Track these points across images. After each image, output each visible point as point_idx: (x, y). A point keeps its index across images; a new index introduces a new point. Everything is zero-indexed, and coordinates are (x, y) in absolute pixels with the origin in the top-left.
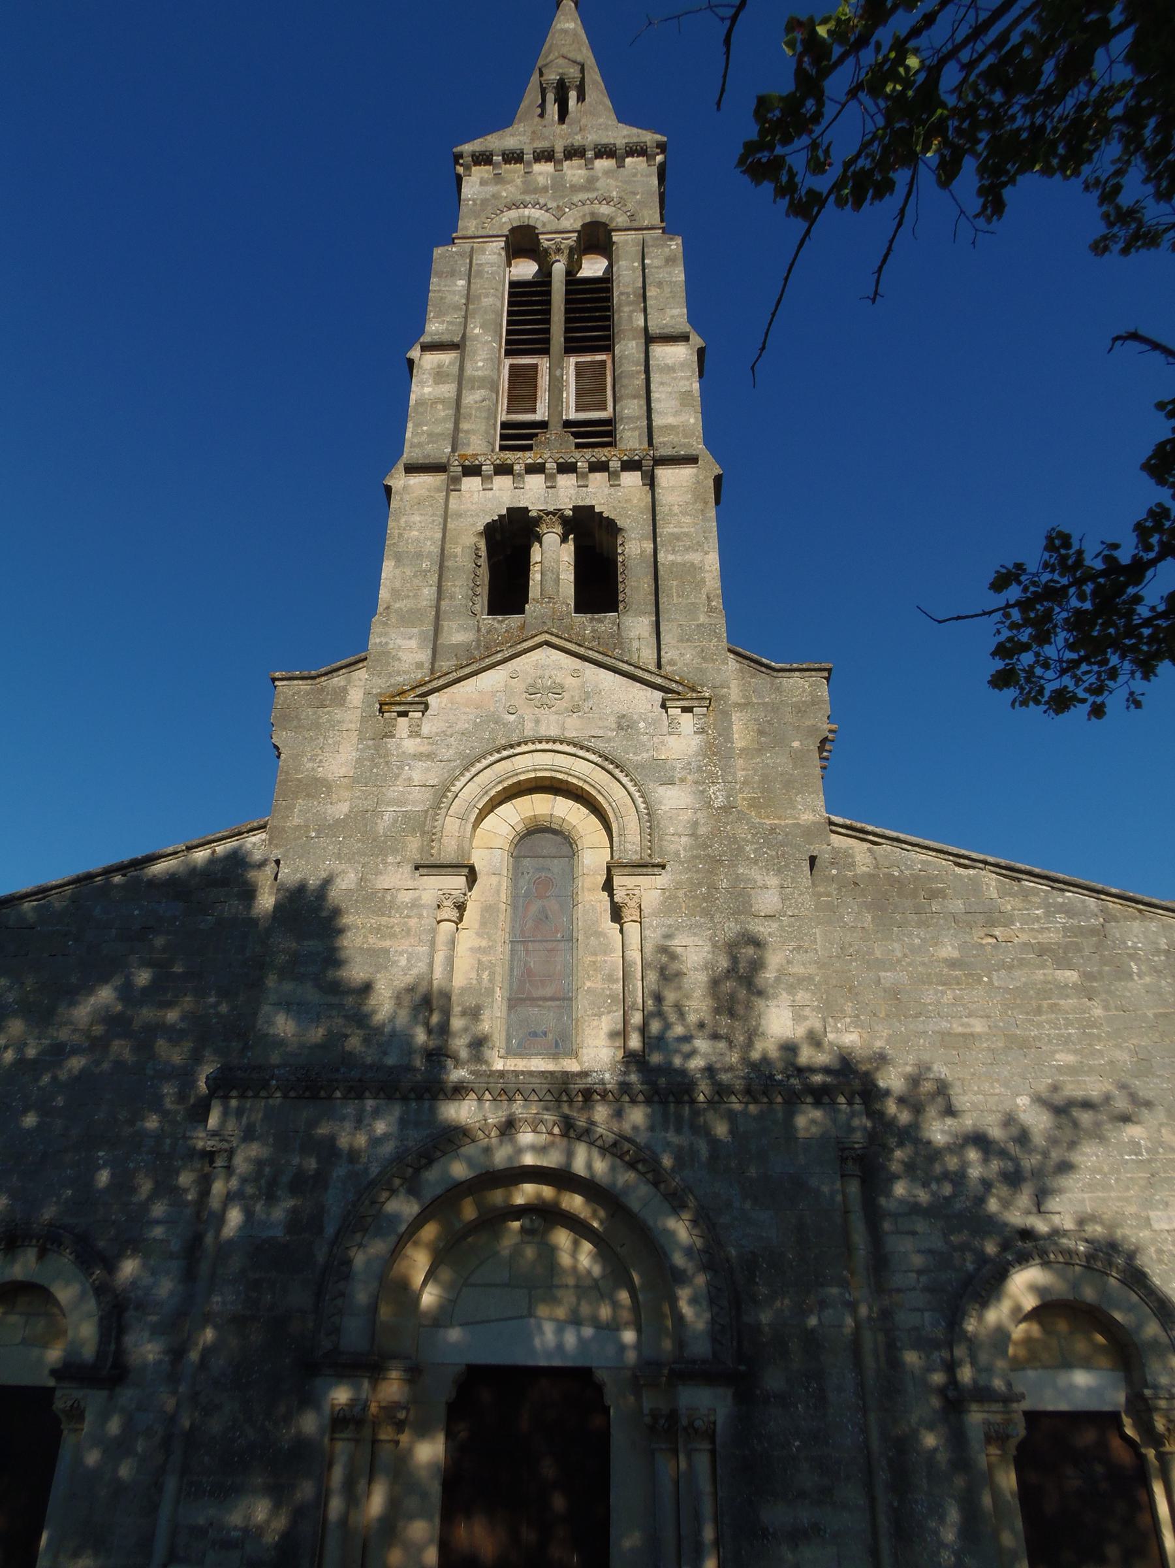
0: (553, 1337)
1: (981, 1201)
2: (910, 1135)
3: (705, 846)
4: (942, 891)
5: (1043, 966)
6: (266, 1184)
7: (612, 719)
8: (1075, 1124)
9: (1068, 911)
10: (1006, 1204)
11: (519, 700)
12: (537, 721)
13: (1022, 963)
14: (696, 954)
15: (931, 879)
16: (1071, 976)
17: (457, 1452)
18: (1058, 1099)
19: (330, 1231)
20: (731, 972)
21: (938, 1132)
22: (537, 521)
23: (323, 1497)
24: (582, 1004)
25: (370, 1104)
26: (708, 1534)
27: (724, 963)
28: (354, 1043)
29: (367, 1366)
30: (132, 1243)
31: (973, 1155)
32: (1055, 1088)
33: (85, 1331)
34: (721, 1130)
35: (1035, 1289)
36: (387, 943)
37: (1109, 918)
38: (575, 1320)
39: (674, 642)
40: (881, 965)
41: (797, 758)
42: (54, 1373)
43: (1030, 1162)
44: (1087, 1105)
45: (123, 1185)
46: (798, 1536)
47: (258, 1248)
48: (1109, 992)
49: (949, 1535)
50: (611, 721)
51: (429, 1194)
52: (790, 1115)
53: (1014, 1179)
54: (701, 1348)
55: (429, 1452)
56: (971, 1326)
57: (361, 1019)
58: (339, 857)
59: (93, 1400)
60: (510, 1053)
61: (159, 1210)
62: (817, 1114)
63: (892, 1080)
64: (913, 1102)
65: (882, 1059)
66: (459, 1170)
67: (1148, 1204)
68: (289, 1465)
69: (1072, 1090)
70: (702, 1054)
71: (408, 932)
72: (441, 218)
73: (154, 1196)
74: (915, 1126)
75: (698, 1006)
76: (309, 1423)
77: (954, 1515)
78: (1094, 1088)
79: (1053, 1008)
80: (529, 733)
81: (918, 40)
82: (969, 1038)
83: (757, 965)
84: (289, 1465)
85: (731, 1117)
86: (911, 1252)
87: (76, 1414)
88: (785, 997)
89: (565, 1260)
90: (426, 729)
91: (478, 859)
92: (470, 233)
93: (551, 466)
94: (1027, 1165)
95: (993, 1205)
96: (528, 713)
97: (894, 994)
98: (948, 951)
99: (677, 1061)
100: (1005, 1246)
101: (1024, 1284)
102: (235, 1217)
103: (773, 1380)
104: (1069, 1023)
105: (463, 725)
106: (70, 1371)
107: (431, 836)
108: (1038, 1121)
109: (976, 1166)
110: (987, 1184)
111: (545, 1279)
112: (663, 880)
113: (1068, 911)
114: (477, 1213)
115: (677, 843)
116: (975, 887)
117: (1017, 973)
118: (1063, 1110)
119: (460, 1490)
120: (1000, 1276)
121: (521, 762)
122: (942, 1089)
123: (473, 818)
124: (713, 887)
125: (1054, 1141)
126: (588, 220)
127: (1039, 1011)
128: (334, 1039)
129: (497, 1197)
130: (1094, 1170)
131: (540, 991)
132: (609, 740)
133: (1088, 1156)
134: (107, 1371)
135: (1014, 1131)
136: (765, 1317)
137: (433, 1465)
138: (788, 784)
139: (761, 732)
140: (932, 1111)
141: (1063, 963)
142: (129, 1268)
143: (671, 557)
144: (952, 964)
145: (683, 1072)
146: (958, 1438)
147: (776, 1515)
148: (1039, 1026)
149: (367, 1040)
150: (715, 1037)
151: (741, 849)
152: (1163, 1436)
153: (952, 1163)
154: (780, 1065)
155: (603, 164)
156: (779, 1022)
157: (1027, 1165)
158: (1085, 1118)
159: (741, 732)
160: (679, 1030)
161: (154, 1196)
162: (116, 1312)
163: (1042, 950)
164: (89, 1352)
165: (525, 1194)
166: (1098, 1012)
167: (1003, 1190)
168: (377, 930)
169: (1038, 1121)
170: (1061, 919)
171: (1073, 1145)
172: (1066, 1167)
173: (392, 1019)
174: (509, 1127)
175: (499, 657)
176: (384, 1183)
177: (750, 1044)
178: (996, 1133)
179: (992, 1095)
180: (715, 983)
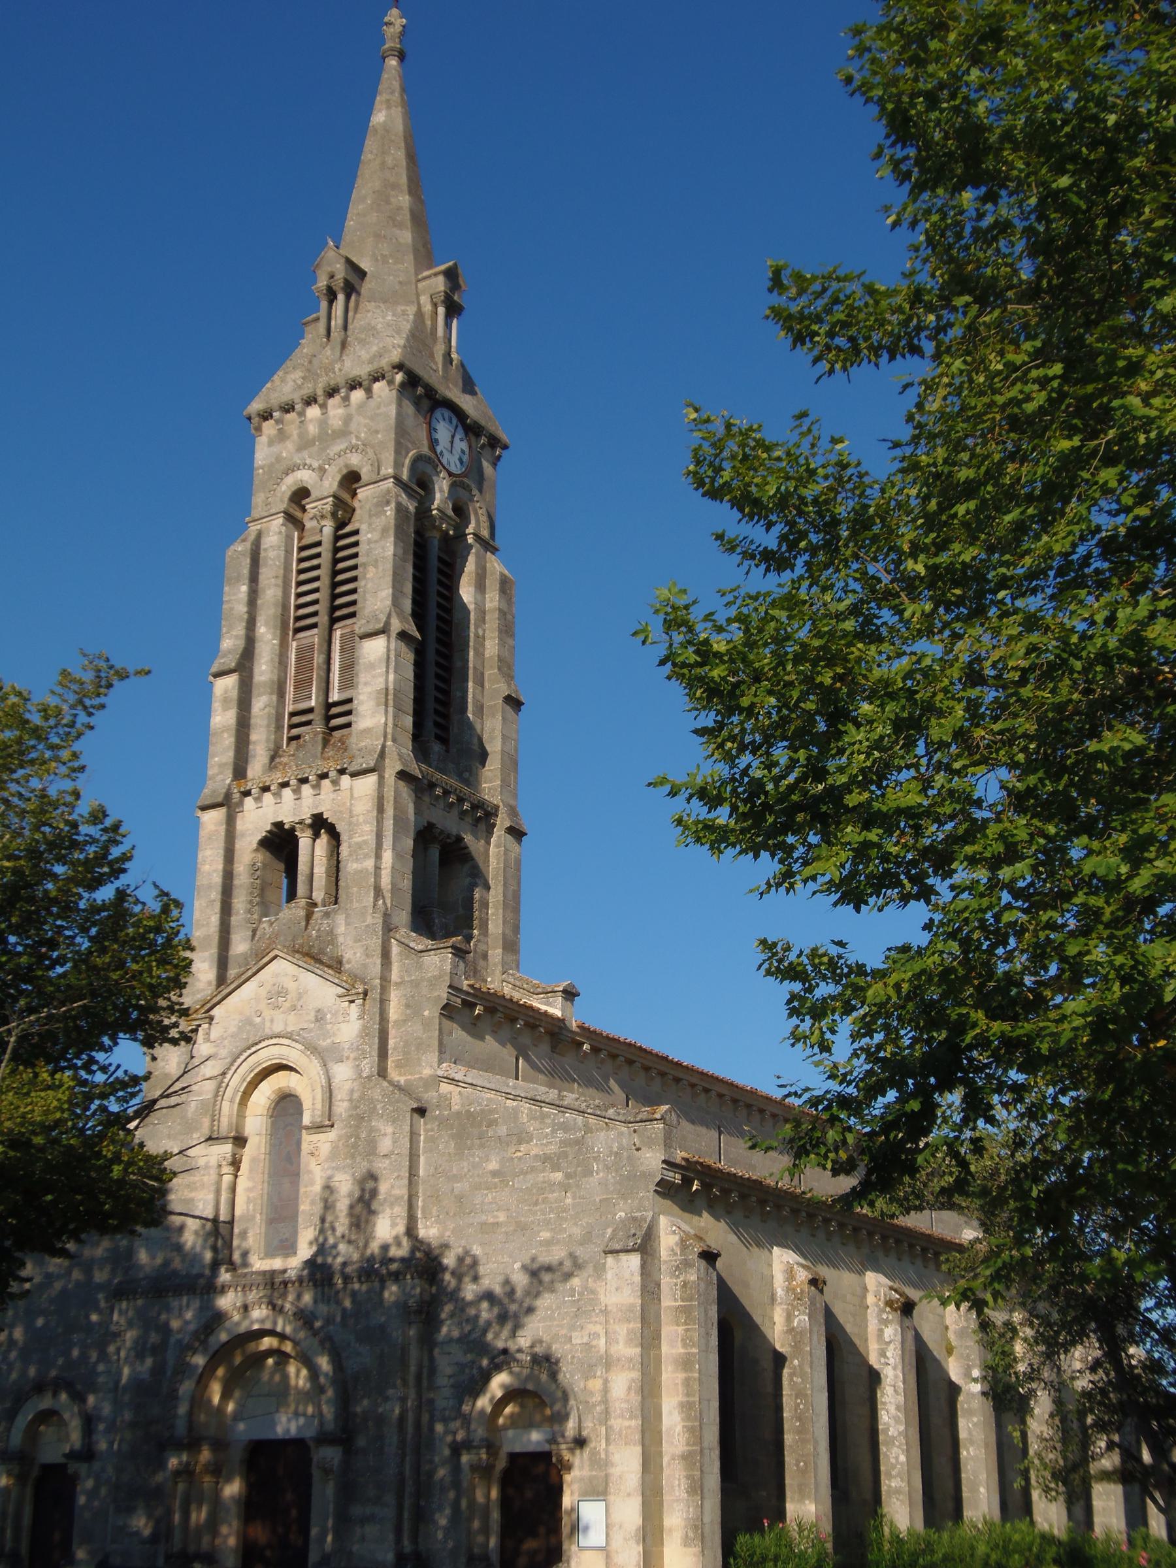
0: (286, 1425)
1: (485, 1332)
2: (454, 1295)
3: (356, 1107)
4: (496, 1120)
5: (543, 1171)
6: (140, 1351)
7: (313, 1014)
8: (541, 1282)
9: (565, 1127)
10: (497, 1335)
11: (263, 1006)
12: (272, 1021)
13: (533, 1169)
14: (345, 1185)
15: (492, 1111)
16: (558, 1176)
17: (252, 1488)
18: (535, 1266)
19: (169, 1373)
20: (361, 1199)
21: (469, 1291)
22: (293, 829)
23: (169, 1512)
24: (301, 1226)
25: (185, 1299)
26: (330, 1523)
27: (357, 1194)
28: (177, 1264)
29: (192, 1444)
30: (92, 1387)
31: (485, 1305)
32: (533, 1260)
33: (75, 1437)
34: (347, 1303)
35: (503, 1386)
36: (193, 1195)
37: (588, 1129)
38: (296, 1414)
39: (350, 943)
41: (426, 1024)
42: (65, 1455)
43: (513, 1307)
44: (549, 1269)
45: (84, 1356)
46: (365, 1520)
47: (137, 1384)
48: (578, 1186)
49: (443, 1522)
50: (312, 1017)
51: (211, 1351)
52: (383, 1288)
53: (503, 1318)
54: (330, 1426)
55: (232, 1489)
56: (466, 1408)
57: (179, 1248)
58: (169, 1137)
59: (83, 1468)
60: (269, 1254)
61: (101, 1368)
62: (394, 1288)
63: (449, 1260)
64: (458, 1275)
65: (446, 1246)
66: (224, 1337)
67: (573, 1328)
68: (155, 1497)
69: (545, 1259)
70: (345, 1252)
71: (203, 1186)
72: (240, 476)
73: (98, 1361)
74: (458, 1289)
75: (342, 1225)
76: (159, 1477)
77: (448, 1511)
78: (556, 1254)
79: (545, 1200)
80: (268, 1032)
82: (497, 1224)
83: (374, 1193)
84: (155, 1497)
85: (354, 1294)
86: (445, 1367)
88: (388, 1210)
89: (293, 1382)
90: (213, 1036)
92: (257, 516)
93: (293, 782)
94: (510, 1309)
95: (490, 1336)
96: (267, 1014)
97: (460, 1199)
98: (493, 1165)
99: (330, 1260)
100: (492, 1360)
101: (499, 1382)
102: (126, 1371)
103: (361, 1442)
104: (551, 1211)
105: (233, 1029)
106: (73, 1455)
107: (215, 1118)
108: (521, 1280)
109: (486, 1312)
110: (489, 1324)
111: (282, 1392)
112: (332, 1135)
113: (565, 1127)
114: (241, 1357)
116: (516, 1111)
117: (529, 1177)
118: (534, 1273)
119: (250, 1507)
120: (486, 1378)
121: (263, 1054)
122: (475, 1263)
123: (238, 1099)
124: (358, 1137)
125: (527, 1293)
126: (345, 471)
127: (536, 1204)
128: (166, 1263)
129: (252, 1347)
130: (547, 1309)
131: (281, 1214)
132: (311, 1031)
133: (545, 1302)
134: (87, 1454)
135: (508, 1289)
136: (359, 1409)
137: (232, 1498)
138: (419, 1047)
139: (408, 1006)
140: (467, 1279)
141: (556, 1168)
142: (91, 1400)
143: (355, 866)
144: (495, 1174)
145: (330, 1266)
146: (456, 1469)
147: (357, 1510)
148: (535, 1213)
149: (183, 1261)
150: (350, 1242)
151: (375, 1108)
153: (472, 1312)
154: (378, 1259)
155: (358, 395)
156: (386, 1228)
157: (510, 1309)
158: (546, 1277)
160: (331, 1241)
161: (98, 1361)
162: (89, 1422)
163: (545, 1159)
164: (78, 1445)
165: (267, 1343)
166: (569, 1201)
167: (496, 1327)
168: (188, 1186)
169: (521, 1280)
170: (560, 1134)
171: (537, 1295)
172: (530, 1310)
173: (193, 1248)
174: (246, 1308)
175: (250, 973)
176: (187, 1348)
177: (366, 1245)
178: (498, 1290)
179: (501, 1268)
180: (351, 1207)
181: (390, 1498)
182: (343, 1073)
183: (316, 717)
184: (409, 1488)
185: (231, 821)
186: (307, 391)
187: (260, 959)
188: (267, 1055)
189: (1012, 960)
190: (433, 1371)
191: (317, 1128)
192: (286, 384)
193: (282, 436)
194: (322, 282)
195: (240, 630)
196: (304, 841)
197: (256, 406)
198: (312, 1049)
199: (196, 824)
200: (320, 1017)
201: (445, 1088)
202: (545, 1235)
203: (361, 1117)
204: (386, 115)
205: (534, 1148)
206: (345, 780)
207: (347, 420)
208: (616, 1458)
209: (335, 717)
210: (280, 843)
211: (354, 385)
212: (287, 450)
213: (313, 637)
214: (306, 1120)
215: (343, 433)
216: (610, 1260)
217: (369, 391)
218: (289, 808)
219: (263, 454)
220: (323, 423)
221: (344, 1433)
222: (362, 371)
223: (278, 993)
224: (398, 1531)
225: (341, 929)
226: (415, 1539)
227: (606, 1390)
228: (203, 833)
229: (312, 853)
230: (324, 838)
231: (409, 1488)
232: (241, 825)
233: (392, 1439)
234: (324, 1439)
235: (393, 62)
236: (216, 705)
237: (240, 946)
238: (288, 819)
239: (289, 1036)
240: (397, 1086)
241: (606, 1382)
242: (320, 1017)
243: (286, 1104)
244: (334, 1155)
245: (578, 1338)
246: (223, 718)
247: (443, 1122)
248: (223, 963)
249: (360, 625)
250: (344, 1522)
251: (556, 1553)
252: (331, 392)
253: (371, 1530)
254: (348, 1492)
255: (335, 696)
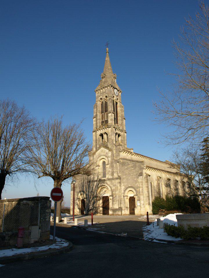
9: (133, 163)
16: (133, 168)
40: (122, 169)
46: (115, 204)
72: (95, 98)
81: (58, 238)
87: (3, 216)
91: (100, 165)
98: (126, 168)
103: (114, 196)
113: (133, 163)
115: (110, 162)
116: (128, 162)
141: (133, 168)
144: (126, 168)
147: (114, 203)
152: (103, 199)
155: (106, 88)
159: (114, 152)
181: (118, 202)
182: (110, 159)
183: (104, 122)
184: (119, 201)
185: (96, 133)
186: (101, 88)
187: (100, 148)
188: (102, 157)
189: (192, 169)
190: (121, 189)
191: (107, 165)
192: (99, 87)
193: (98, 93)
194: (102, 77)
195: (95, 113)
196: (104, 135)
197: (96, 90)
198: (106, 156)
199: (93, 134)
200: (107, 153)
201: (120, 160)
202: (132, 175)
203: (112, 163)
204: (107, 59)
205: (130, 166)
206: (108, 128)
207: (105, 91)
208: (141, 197)
209: (107, 122)
210: (102, 135)
211: (106, 87)
212: (99, 94)
213: (103, 114)
214: (106, 164)
215: (105, 92)
216: (139, 177)
217: (107, 88)
218: (102, 131)
219: (97, 95)
220: (103, 91)
221: (112, 196)
222: (106, 86)
223: (102, 151)
224: (119, 205)
225: (108, 144)
226: (120, 206)
227: (139, 190)
228: (93, 135)
229: (105, 136)
230: (106, 134)
231: (119, 201)
232: (97, 134)
233: (117, 196)
234: (110, 196)
235: (107, 53)
236: (94, 121)
237: (98, 146)
238: (102, 133)
239: (104, 155)
240: (115, 160)
241: (139, 189)
242: (107, 153)
243: (104, 162)
244: (109, 167)
245: (136, 185)
246: (94, 123)
247: (120, 163)
248: (96, 148)
249: (108, 112)
250: (113, 204)
251: (1, 249)
252: (104, 88)
253: (116, 205)
254: (113, 201)
255: (106, 120)
